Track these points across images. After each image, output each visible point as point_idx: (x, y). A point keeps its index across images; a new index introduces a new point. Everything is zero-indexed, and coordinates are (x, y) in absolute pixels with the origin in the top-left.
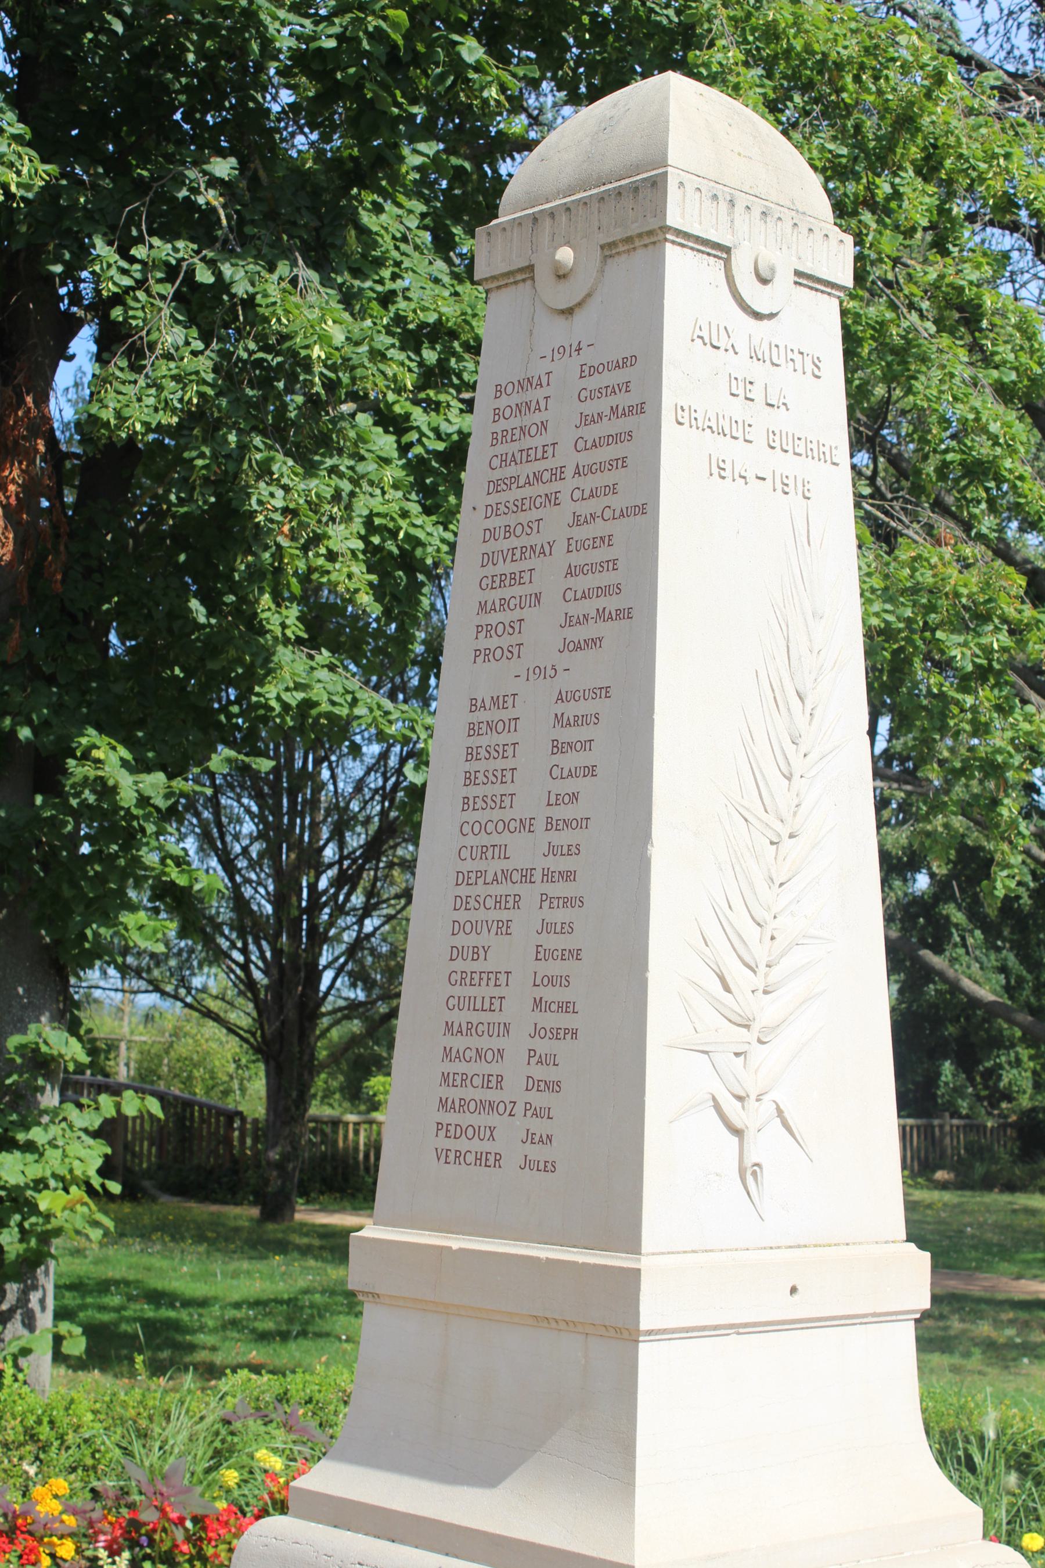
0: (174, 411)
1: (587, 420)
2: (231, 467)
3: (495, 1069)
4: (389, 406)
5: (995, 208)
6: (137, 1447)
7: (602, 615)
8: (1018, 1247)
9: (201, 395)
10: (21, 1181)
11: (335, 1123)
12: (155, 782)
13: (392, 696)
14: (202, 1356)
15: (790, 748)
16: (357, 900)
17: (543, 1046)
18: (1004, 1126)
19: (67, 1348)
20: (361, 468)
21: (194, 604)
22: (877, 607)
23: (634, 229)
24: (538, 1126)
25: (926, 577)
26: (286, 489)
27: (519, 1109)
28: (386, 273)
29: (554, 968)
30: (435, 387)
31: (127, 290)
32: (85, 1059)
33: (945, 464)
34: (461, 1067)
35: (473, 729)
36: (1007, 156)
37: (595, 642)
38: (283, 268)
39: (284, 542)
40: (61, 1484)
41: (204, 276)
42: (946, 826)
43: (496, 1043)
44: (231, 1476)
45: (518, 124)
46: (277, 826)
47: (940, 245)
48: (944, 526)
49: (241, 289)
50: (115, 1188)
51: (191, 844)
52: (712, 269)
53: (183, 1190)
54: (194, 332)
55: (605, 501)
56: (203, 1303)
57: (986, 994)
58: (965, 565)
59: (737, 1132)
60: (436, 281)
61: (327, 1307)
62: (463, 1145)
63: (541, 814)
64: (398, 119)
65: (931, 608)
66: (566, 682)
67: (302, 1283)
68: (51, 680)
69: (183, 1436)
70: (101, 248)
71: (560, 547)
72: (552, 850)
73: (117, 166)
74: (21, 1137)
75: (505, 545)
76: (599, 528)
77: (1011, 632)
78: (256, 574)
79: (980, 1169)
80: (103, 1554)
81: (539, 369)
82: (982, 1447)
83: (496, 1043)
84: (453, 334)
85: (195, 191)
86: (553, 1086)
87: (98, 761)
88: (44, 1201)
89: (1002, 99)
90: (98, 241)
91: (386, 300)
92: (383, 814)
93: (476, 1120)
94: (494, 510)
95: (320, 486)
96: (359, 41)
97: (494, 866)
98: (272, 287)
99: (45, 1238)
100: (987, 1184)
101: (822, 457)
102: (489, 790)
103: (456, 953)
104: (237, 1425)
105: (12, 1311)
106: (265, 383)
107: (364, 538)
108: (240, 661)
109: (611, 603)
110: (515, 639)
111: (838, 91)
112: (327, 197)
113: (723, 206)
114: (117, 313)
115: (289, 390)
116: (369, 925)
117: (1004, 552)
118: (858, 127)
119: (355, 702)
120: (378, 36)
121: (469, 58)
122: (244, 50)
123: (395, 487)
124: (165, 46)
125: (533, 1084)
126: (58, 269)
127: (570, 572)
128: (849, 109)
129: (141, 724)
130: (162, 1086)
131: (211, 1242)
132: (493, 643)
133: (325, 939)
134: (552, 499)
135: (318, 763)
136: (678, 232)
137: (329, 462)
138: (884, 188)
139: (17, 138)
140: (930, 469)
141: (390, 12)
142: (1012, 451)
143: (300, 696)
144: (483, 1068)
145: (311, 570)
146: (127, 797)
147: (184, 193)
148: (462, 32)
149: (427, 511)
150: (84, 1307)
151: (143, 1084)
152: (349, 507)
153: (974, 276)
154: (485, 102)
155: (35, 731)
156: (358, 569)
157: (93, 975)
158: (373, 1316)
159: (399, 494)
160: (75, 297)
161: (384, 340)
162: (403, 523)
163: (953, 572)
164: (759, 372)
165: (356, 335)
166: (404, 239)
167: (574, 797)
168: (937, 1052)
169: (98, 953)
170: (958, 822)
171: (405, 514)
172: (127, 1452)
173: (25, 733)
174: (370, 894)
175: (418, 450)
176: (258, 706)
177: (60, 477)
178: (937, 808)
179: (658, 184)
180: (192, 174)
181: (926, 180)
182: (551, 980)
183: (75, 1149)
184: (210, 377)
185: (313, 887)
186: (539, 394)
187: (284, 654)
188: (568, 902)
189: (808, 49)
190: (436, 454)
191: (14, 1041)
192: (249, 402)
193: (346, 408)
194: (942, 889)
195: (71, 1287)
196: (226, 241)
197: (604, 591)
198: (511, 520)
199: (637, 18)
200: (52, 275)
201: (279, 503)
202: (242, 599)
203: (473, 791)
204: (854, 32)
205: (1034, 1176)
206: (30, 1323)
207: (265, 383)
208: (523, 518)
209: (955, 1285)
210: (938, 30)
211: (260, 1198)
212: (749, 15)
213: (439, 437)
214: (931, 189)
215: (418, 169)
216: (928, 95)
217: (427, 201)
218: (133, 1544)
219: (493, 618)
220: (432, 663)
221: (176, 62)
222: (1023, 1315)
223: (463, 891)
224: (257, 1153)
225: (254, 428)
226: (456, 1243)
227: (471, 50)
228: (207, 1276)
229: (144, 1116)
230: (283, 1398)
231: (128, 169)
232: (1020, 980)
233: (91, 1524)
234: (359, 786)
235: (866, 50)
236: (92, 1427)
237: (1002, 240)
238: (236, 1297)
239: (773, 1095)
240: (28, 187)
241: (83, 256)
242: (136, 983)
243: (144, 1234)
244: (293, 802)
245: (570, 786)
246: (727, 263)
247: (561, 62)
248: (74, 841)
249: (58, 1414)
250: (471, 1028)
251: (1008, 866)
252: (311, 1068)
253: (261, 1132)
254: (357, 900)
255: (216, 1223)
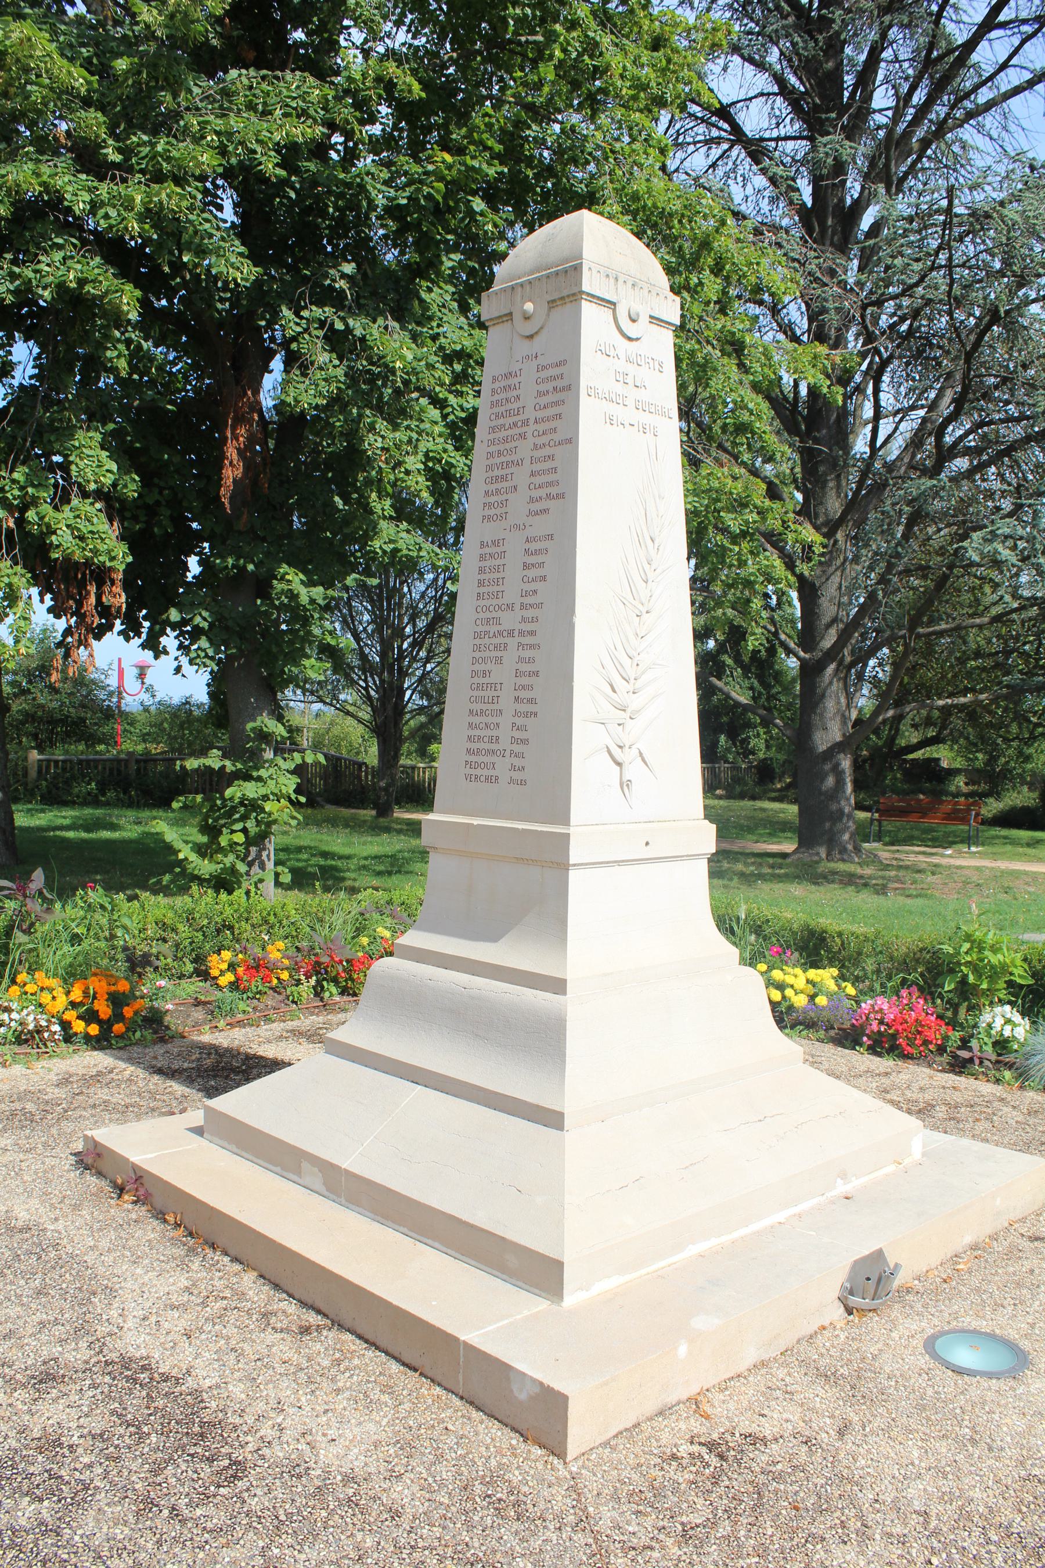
0: (324, 397)
1: (540, 394)
2: (354, 426)
3: (494, 733)
4: (437, 394)
5: (752, 292)
6: (318, 926)
7: (549, 496)
8: (756, 827)
9: (338, 388)
10: (256, 796)
11: (413, 768)
12: (318, 592)
13: (440, 547)
14: (349, 883)
15: (647, 567)
16: (423, 654)
17: (519, 721)
18: (750, 768)
19: (282, 879)
20: (422, 426)
21: (337, 499)
22: (690, 499)
23: (565, 293)
24: (517, 762)
25: (716, 484)
26: (383, 437)
27: (507, 753)
28: (434, 324)
29: (525, 681)
30: (460, 384)
31: (299, 334)
32: (285, 734)
33: (725, 425)
34: (477, 732)
35: (482, 558)
36: (758, 264)
37: (545, 511)
38: (380, 321)
39: (383, 466)
40: (281, 945)
41: (339, 326)
42: (724, 614)
43: (495, 720)
44: (365, 940)
45: (503, 246)
46: (381, 617)
47: (723, 311)
48: (724, 457)
49: (358, 332)
50: (303, 799)
51: (337, 625)
52: (606, 314)
53: (338, 802)
54: (334, 355)
55: (550, 437)
56: (348, 857)
57: (743, 699)
58: (735, 478)
59: (619, 764)
60: (461, 328)
61: (410, 859)
62: (479, 772)
63: (518, 601)
64: (440, 241)
65: (718, 500)
66: (530, 532)
67: (398, 847)
68: (264, 539)
69: (341, 920)
70: (286, 312)
71: (527, 461)
72: (524, 620)
73: (293, 269)
74: (255, 774)
75: (498, 460)
76: (547, 451)
77: (758, 513)
78: (369, 482)
79: (738, 789)
80: (303, 977)
81: (515, 367)
82: (738, 923)
83: (495, 720)
84: (470, 356)
85: (334, 281)
86: (525, 742)
87: (289, 581)
88: (268, 807)
89: (755, 235)
90: (284, 308)
91: (434, 338)
92: (436, 610)
93: (486, 759)
94: (492, 442)
95: (400, 435)
96: (418, 200)
97: (494, 629)
98: (375, 331)
99: (269, 824)
100: (742, 796)
101: (663, 414)
102: (491, 589)
103: (474, 674)
104: (367, 916)
105: (254, 861)
106: (371, 382)
107: (424, 464)
108: (361, 528)
109: (554, 491)
110: (503, 510)
111: (671, 228)
112: (403, 283)
113: (612, 281)
114: (294, 346)
115: (384, 385)
116: (429, 667)
117: (755, 473)
118: (680, 248)
119: (420, 549)
120: (429, 197)
121: (477, 209)
122: (359, 206)
123: (440, 435)
124: (318, 204)
125: (515, 740)
126: (263, 323)
127: (532, 474)
128: (676, 238)
129: (310, 562)
130: (325, 750)
131: (352, 828)
132: (492, 512)
133: (407, 674)
134: (523, 436)
135: (402, 583)
136: (588, 294)
137: (405, 423)
138: (694, 280)
139: (241, 254)
140: (717, 428)
141: (435, 184)
142: (760, 418)
143: (392, 546)
144: (489, 733)
145: (397, 480)
146: (304, 599)
147: (328, 282)
148: (473, 195)
149: (457, 449)
150: (289, 860)
151: (316, 747)
152: (416, 447)
153: (741, 327)
154: (486, 232)
155: (256, 566)
156: (421, 479)
157: (288, 693)
158: (432, 857)
159: (442, 440)
160: (273, 339)
161: (433, 359)
162: (445, 456)
163: (729, 481)
164: (631, 369)
165: (419, 356)
166: (444, 306)
167: (535, 592)
168: (718, 730)
169: (293, 680)
170: (730, 612)
171: (445, 451)
172: (313, 929)
173: (251, 567)
174: (429, 651)
175: (451, 417)
176: (370, 552)
177: (266, 434)
178: (719, 604)
179: (577, 269)
180: (332, 272)
181: (716, 276)
182: (523, 687)
183: (282, 780)
184: (343, 379)
185: (400, 647)
186: (516, 380)
187: (383, 524)
188: (532, 647)
189: (655, 206)
190: (462, 420)
191: (250, 725)
192: (363, 392)
193: (415, 395)
194: (721, 647)
195: (282, 850)
196: (350, 308)
197: (550, 484)
198: (501, 447)
199: (565, 188)
200: (260, 327)
201: (379, 445)
202: (361, 496)
203: (482, 590)
204: (679, 197)
205: (765, 792)
206: (262, 867)
207: (371, 382)
208: (508, 446)
209: (726, 846)
210: (723, 198)
211: (376, 806)
212: (624, 188)
213: (463, 410)
214: (719, 281)
215: (451, 268)
216: (717, 231)
217: (455, 286)
218: (318, 973)
219: (492, 499)
220: (460, 529)
221: (323, 213)
222: (759, 860)
223: (478, 641)
224: (374, 783)
225: (366, 406)
226: (476, 821)
227: (478, 204)
228: (350, 844)
229: (317, 763)
230: (390, 902)
231: (299, 270)
232: (760, 694)
233: (296, 963)
234: (423, 595)
235: (685, 207)
236: (295, 917)
237: (754, 309)
238: (365, 854)
239: (638, 745)
240: (246, 280)
241: (275, 317)
242: (311, 698)
243: (318, 824)
244: (389, 604)
245: (533, 586)
246: (614, 310)
247: (526, 213)
248: (277, 623)
249: (278, 910)
250: (482, 712)
251: (754, 634)
252: (400, 740)
253: (377, 773)
254: (423, 654)
255: (354, 818)
